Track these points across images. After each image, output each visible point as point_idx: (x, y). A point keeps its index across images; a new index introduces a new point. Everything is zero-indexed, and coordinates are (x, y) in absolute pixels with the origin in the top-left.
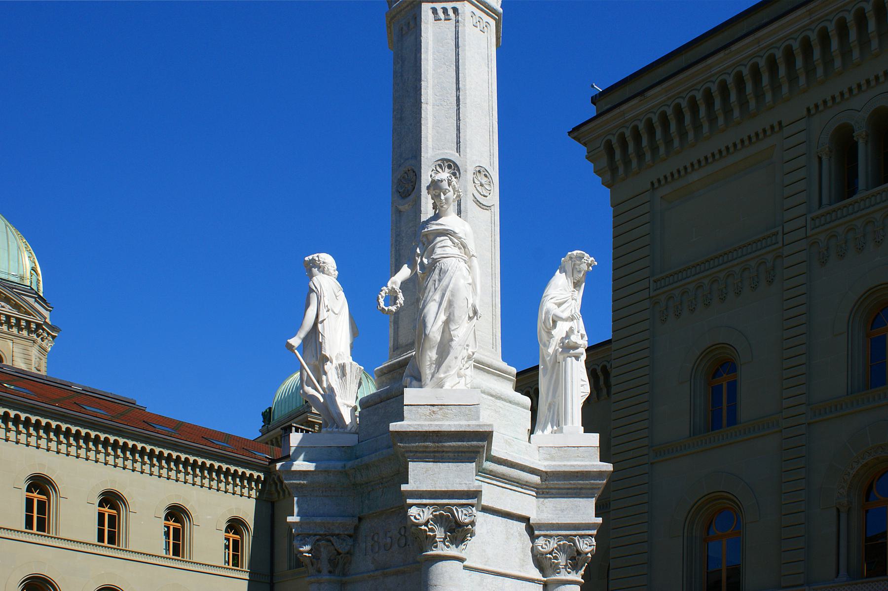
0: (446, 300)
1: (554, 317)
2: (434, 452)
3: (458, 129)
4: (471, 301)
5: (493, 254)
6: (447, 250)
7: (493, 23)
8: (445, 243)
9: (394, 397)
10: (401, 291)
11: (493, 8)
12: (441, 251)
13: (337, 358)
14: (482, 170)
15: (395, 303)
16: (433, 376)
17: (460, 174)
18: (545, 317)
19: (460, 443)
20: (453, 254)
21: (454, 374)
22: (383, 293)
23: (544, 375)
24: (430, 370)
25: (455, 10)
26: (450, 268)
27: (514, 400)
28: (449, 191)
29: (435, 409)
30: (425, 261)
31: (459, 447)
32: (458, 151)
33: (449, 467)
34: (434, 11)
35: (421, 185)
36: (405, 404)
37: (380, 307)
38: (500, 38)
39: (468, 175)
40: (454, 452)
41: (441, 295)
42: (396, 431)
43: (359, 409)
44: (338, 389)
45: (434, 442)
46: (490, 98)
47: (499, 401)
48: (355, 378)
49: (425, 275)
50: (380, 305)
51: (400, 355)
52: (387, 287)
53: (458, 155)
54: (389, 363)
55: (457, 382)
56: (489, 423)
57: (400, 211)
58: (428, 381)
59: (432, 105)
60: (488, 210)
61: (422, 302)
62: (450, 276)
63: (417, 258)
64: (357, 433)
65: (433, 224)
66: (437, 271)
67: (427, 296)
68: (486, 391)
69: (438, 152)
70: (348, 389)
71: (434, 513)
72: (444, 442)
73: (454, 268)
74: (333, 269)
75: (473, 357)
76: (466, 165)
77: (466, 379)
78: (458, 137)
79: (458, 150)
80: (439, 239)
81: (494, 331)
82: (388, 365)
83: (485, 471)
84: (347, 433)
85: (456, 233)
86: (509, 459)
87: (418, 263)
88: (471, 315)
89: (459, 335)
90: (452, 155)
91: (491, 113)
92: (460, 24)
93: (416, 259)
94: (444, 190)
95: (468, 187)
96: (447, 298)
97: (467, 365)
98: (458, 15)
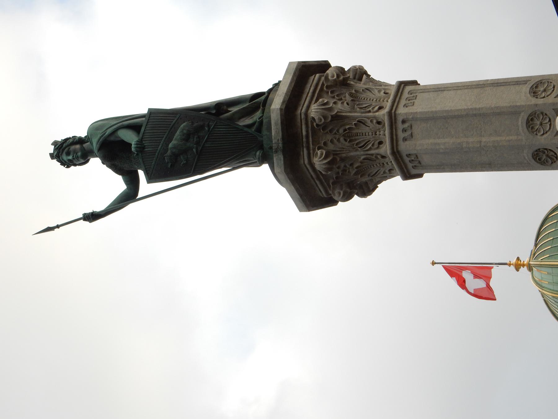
90: (521, 120)
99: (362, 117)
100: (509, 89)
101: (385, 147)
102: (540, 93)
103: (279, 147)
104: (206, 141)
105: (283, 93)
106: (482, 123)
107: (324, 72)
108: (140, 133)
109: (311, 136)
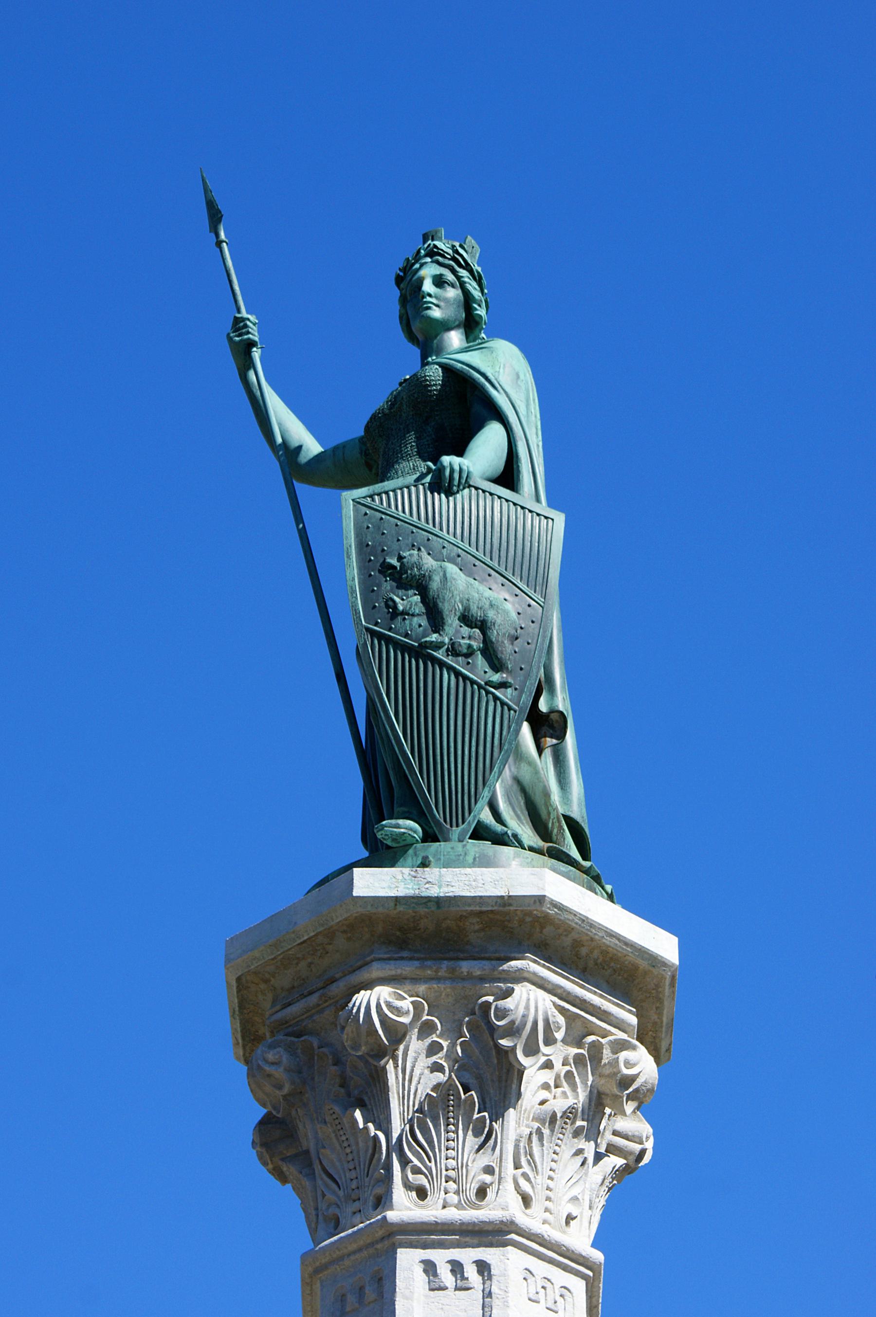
7: (579, 1286)
11: (581, 1255)
25: (483, 1267)
34: (430, 1268)
38: (597, 1307)
71: (415, 566)
92: (496, 1302)
98: (490, 1277)
99: (501, 1142)
101: (408, 1204)
103: (427, 886)
104: (458, 674)
105: (589, 910)
107: (640, 1039)
108: (492, 484)
109: (346, 1232)
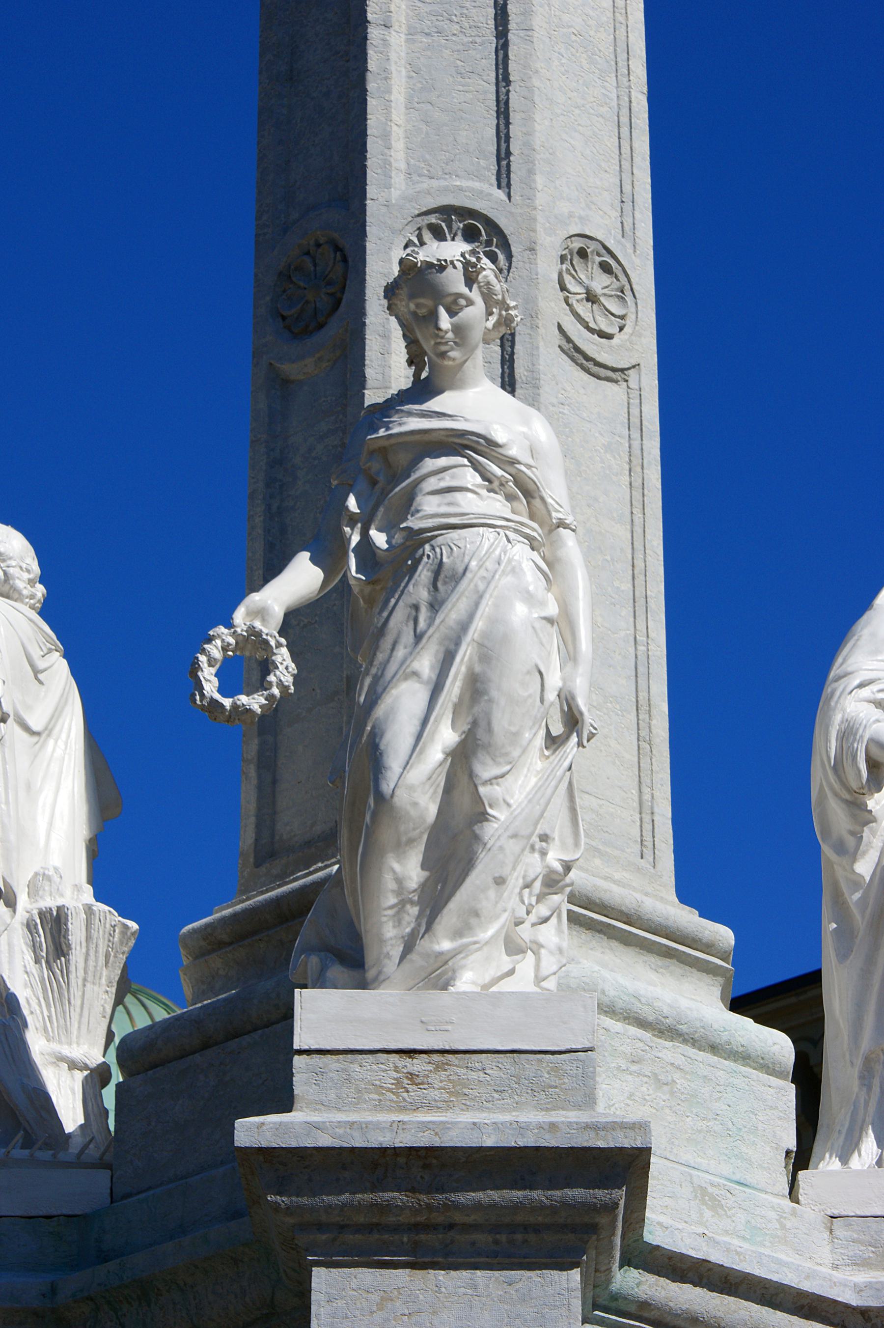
0: (460, 677)
1: (876, 753)
2: (416, 1227)
3: (503, 111)
4: (554, 681)
5: (638, 530)
6: (462, 503)
8: (453, 477)
9: (255, 1030)
10: (283, 641)
12: (439, 505)
13: (33, 890)
14: (592, 247)
15: (263, 685)
16: (409, 947)
17: (509, 257)
18: (840, 748)
19: (518, 1195)
20: (485, 516)
21: (494, 937)
22: (215, 650)
23: (843, 955)
24: (398, 920)
26: (474, 563)
27: (729, 1043)
28: (470, 303)
29: (418, 1065)
30: (379, 539)
31: (517, 1207)
32: (504, 182)
33: (475, 1287)
35: (364, 294)
36: (296, 1046)
37: (202, 696)
39: (539, 261)
40: (496, 1229)
41: (441, 656)
42: (260, 1150)
43: (117, 1076)
44: (34, 1003)
45: (413, 1190)
46: (620, 18)
47: (669, 1044)
48: (102, 960)
49: (378, 587)
50: (201, 688)
51: (282, 878)
52: (229, 625)
53: (504, 197)
54: (239, 907)
55: (506, 968)
56: (634, 1114)
57: (286, 382)
58: (390, 966)
59: (404, 29)
60: (616, 382)
61: (368, 681)
62: (476, 590)
63: (347, 530)
64: (109, 1167)
65: (410, 414)
66: (424, 574)
67: (388, 661)
68: (620, 1004)
69: (426, 184)
70: (76, 1002)
72: (454, 1190)
73: (490, 565)
74: (26, 576)
75: (568, 880)
76: (534, 231)
77: (538, 960)
78: (503, 136)
79: (504, 179)
80: (430, 464)
81: (647, 797)
82: (235, 915)
83: (621, 1304)
84: (68, 1165)
85: (497, 445)
86: (716, 1257)
87: (353, 544)
88: (557, 729)
89: (511, 801)
91: (622, 64)
93: (342, 533)
94: (449, 299)
95: (542, 304)
96: (463, 669)
97: (543, 910)
100: (603, 164)
102: (583, 277)
106: (466, 40)
